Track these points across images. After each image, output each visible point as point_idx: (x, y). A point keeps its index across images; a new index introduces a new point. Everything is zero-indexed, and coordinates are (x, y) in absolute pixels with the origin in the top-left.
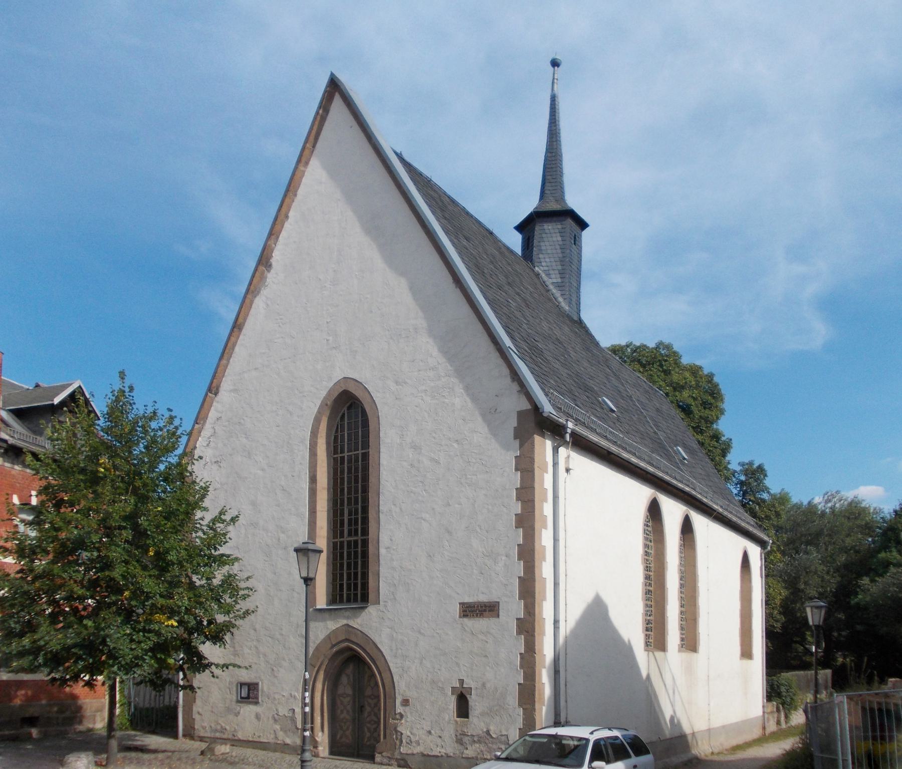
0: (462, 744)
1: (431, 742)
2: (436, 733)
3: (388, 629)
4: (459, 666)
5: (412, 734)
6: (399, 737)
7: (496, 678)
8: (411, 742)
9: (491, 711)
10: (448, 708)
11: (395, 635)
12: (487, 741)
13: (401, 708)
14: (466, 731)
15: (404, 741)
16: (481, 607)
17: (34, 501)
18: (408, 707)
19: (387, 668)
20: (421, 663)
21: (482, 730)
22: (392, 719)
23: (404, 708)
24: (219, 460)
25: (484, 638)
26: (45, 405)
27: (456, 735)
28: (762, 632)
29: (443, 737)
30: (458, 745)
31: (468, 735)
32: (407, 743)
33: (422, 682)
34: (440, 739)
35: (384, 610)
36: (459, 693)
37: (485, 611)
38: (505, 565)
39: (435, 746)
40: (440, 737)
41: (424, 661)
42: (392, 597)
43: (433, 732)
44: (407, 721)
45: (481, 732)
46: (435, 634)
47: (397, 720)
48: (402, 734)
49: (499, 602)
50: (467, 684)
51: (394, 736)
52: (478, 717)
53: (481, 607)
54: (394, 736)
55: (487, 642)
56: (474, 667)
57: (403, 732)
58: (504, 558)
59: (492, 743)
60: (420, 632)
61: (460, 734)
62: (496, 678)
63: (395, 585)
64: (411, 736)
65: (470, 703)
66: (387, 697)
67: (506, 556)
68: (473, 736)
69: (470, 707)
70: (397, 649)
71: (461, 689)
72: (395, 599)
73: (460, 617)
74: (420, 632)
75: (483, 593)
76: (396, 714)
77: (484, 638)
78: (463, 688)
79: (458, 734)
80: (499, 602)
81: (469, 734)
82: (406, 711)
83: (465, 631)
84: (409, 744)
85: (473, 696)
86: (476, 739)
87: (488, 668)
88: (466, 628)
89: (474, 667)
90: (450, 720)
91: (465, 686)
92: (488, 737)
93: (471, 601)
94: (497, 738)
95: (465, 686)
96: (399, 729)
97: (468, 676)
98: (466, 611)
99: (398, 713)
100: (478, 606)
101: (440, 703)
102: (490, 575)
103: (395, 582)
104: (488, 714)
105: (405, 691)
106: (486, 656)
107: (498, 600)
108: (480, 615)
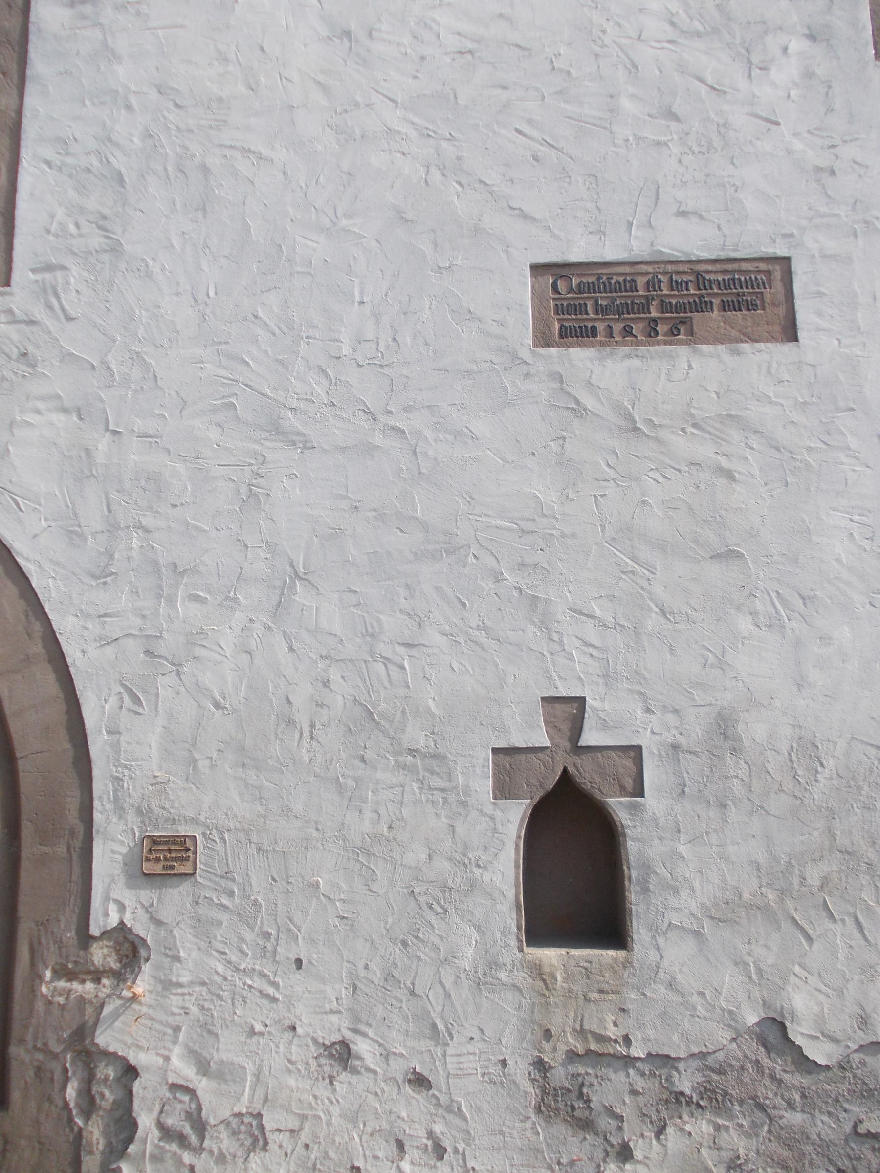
0: (586, 1125)
1: (353, 1118)
2: (387, 1056)
3: (59, 419)
4: (545, 624)
5: (203, 1067)
6: (108, 1096)
7: (800, 684)
8: (201, 1127)
9: (783, 893)
10: (473, 885)
11: (103, 445)
12: (766, 1092)
13: (128, 897)
14: (612, 1032)
15: (146, 1121)
16: (674, 285)
17: (269, 761)
18: (186, 886)
19: (37, 648)
20: (279, 609)
21: (731, 1018)
22: (63, 972)
23: (147, 895)
24: (320, 685)
25: (705, 451)
26: (524, 859)
27: (540, 1065)
28: (517, 867)
29: (438, 1078)
30: (560, 1129)
31: (629, 1061)
32: (167, 1133)
33: (291, 723)
34: (419, 1099)
35: (39, 313)
36: (551, 783)
37: (701, 306)
38: (809, 75)
39: (384, 1149)
40: (420, 1081)
41: (301, 595)
42: (96, 240)
43: (362, 1047)
44: (168, 985)
45: (723, 1036)
46: (378, 439)
47: (97, 976)
48: (131, 1072)
49: (786, 261)
50: (605, 726)
51: (71, 1093)
52: (698, 934)
53: (674, 285)
54: (71, 1093)
55: (729, 475)
56: (653, 622)
57: (136, 1058)
58: (797, 45)
59: (808, 1102)
60: (276, 429)
61: (572, 1056)
62: (800, 684)
63: (120, 179)
64: (203, 1086)
65: (632, 848)
66: (27, 830)
67: (812, 37)
68: (666, 1060)
69: (633, 873)
70: (113, 528)
71: (562, 761)
72: (115, 249)
73: (543, 340)
74: (276, 429)
75: (683, 214)
76: (85, 939)
77: (705, 451)
78: (578, 750)
79: (554, 1058)
80: (786, 261)
81: (637, 1051)
82: (166, 914)
83: (579, 410)
84: (182, 1140)
85: (652, 801)
86: (685, 1083)
87: (744, 624)
88: (589, 402)
89: (653, 622)
90: (494, 964)
91: (590, 737)
92: (777, 1065)
93: (610, 254)
94: (843, 1066)
95: (590, 737)
96: (105, 1039)
97: (608, 677)
98: (579, 309)
99: (106, 934)
100: (652, 285)
101: (417, 854)
102: (726, 124)
103: (119, 161)
104: (764, 909)
105: (160, 786)
106: (730, 555)
107: (781, 250)
108: (673, 332)
